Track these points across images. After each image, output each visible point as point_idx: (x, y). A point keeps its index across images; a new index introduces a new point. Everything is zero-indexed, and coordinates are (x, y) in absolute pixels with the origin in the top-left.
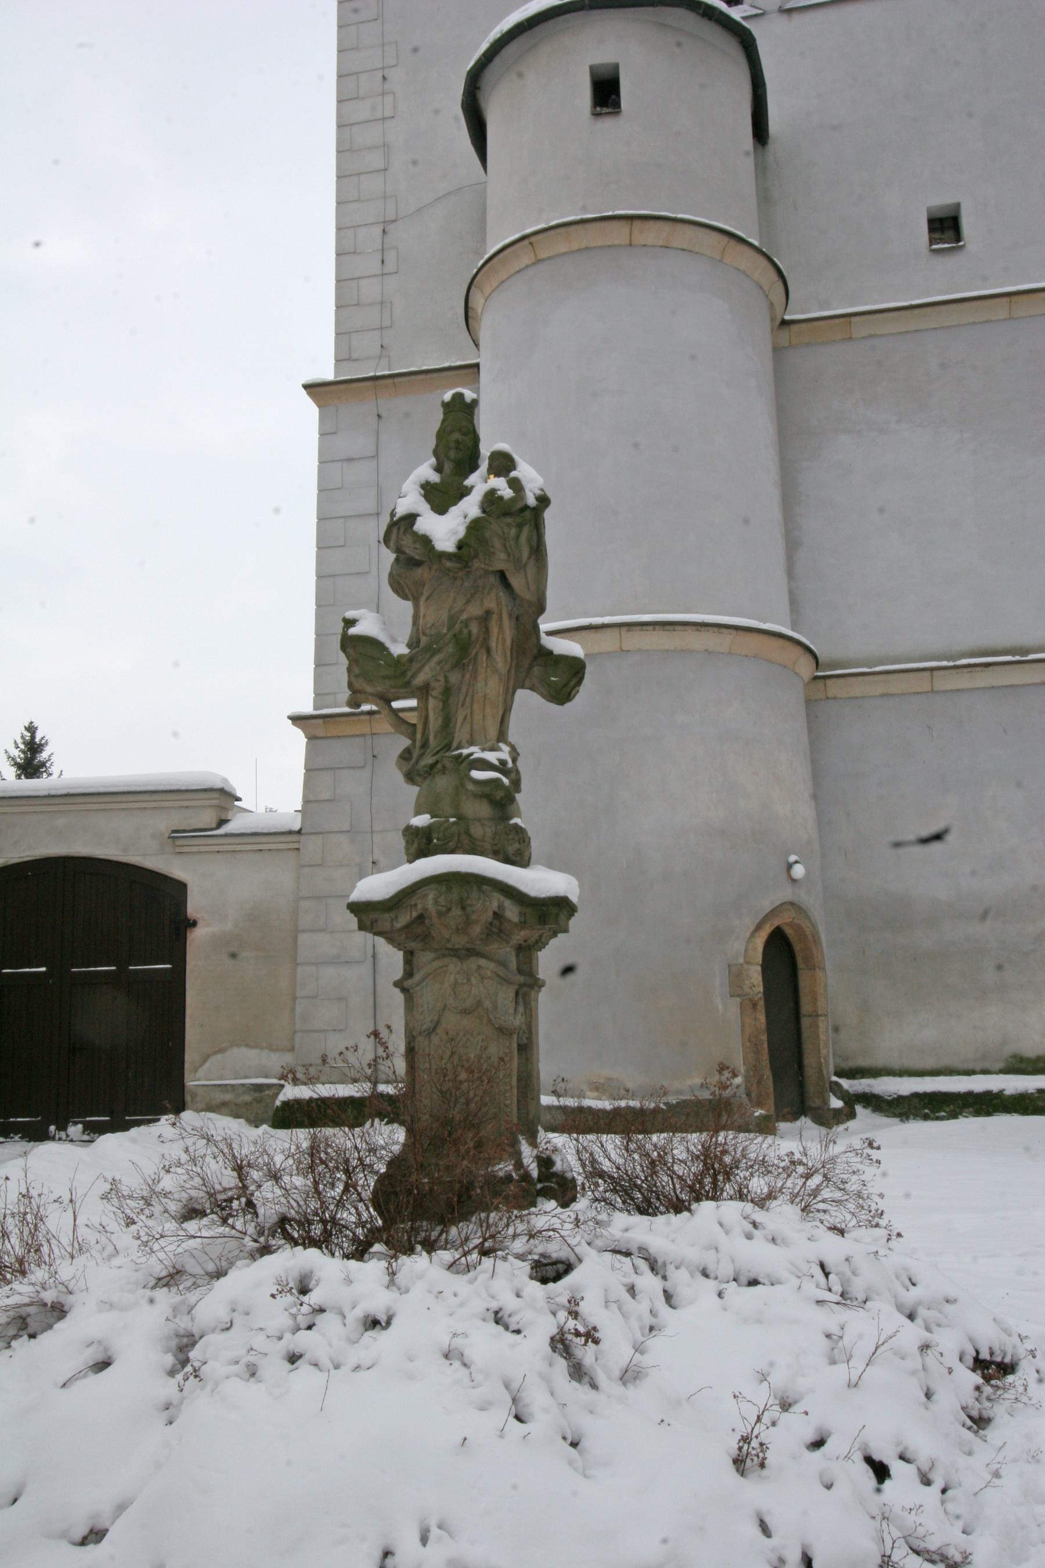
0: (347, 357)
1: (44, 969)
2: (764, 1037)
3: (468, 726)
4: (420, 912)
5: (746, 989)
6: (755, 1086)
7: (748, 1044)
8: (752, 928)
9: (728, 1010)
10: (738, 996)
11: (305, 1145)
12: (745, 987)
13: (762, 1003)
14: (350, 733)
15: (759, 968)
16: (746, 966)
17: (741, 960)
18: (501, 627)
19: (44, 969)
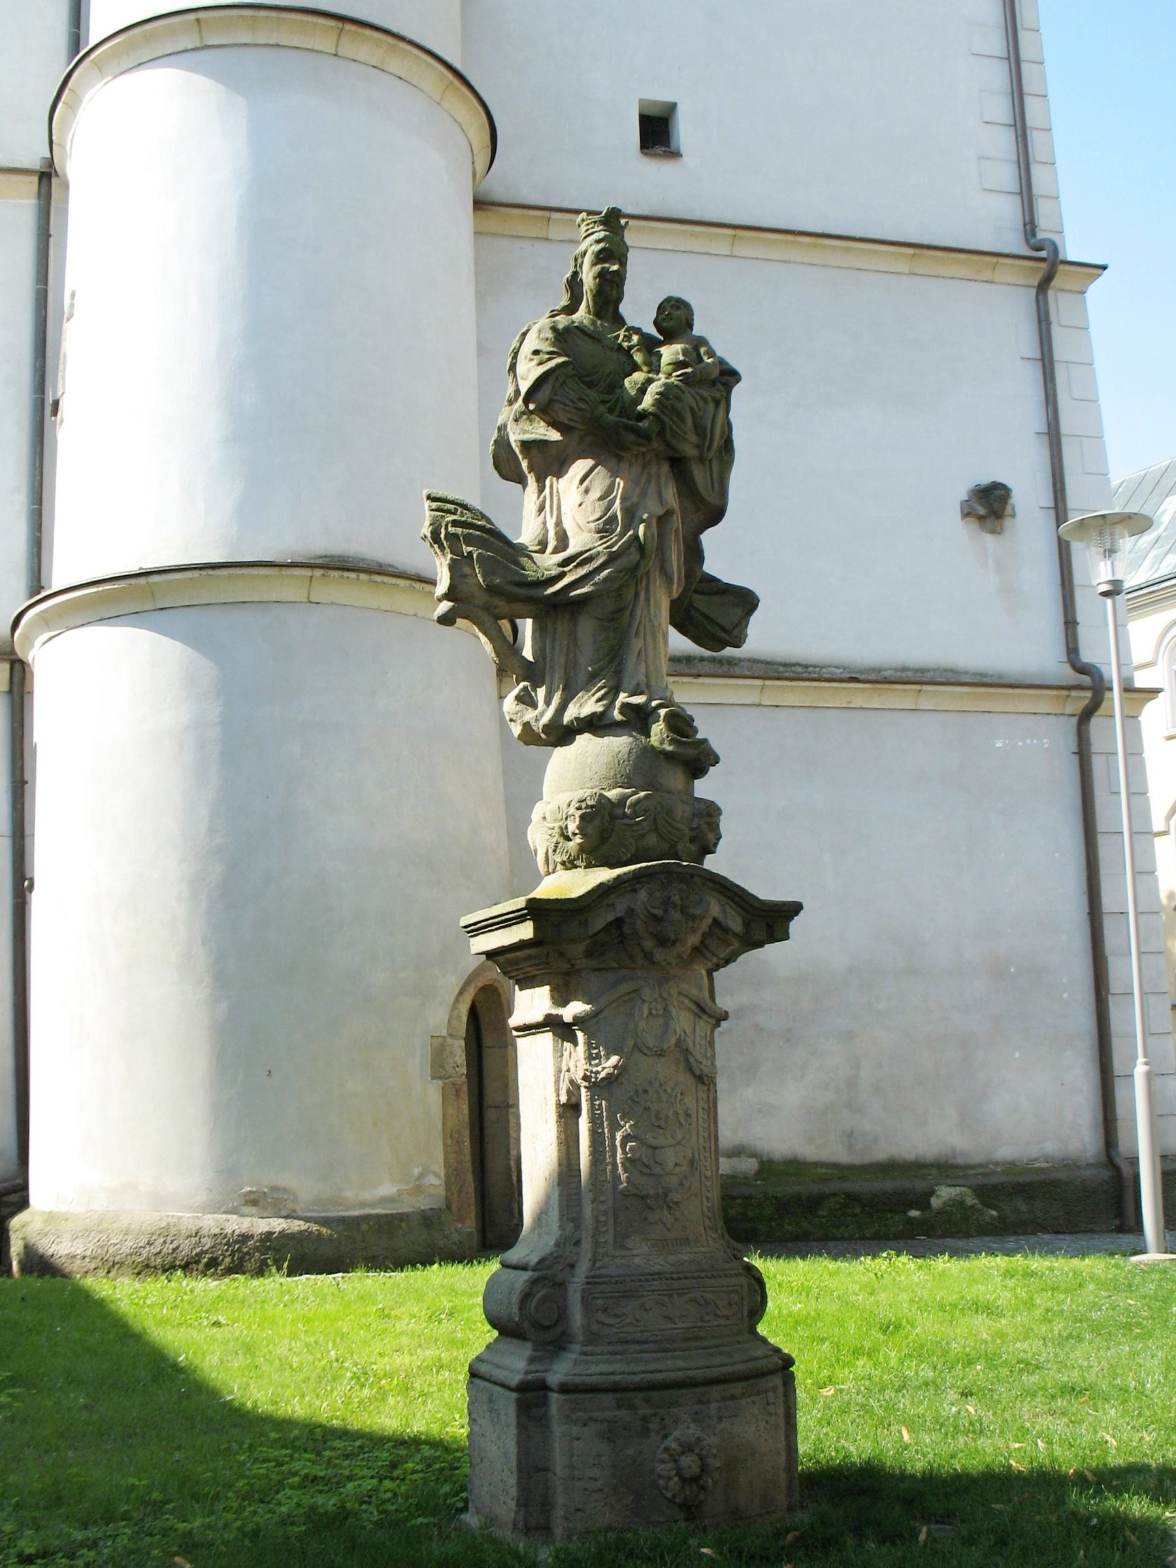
0: (1034, 743)
1: (572, 594)
2: (467, 1133)
3: (533, 555)
4: (619, 915)
5: (451, 1071)
6: (456, 1195)
7: (449, 1141)
8: (456, 992)
9: (433, 1094)
10: (440, 1078)
11: (561, 1397)
12: (447, 1067)
13: (465, 1088)
14: (215, 43)
15: (463, 1043)
16: (449, 1040)
17: (444, 1033)
18: (679, 566)
19: (572, 594)
